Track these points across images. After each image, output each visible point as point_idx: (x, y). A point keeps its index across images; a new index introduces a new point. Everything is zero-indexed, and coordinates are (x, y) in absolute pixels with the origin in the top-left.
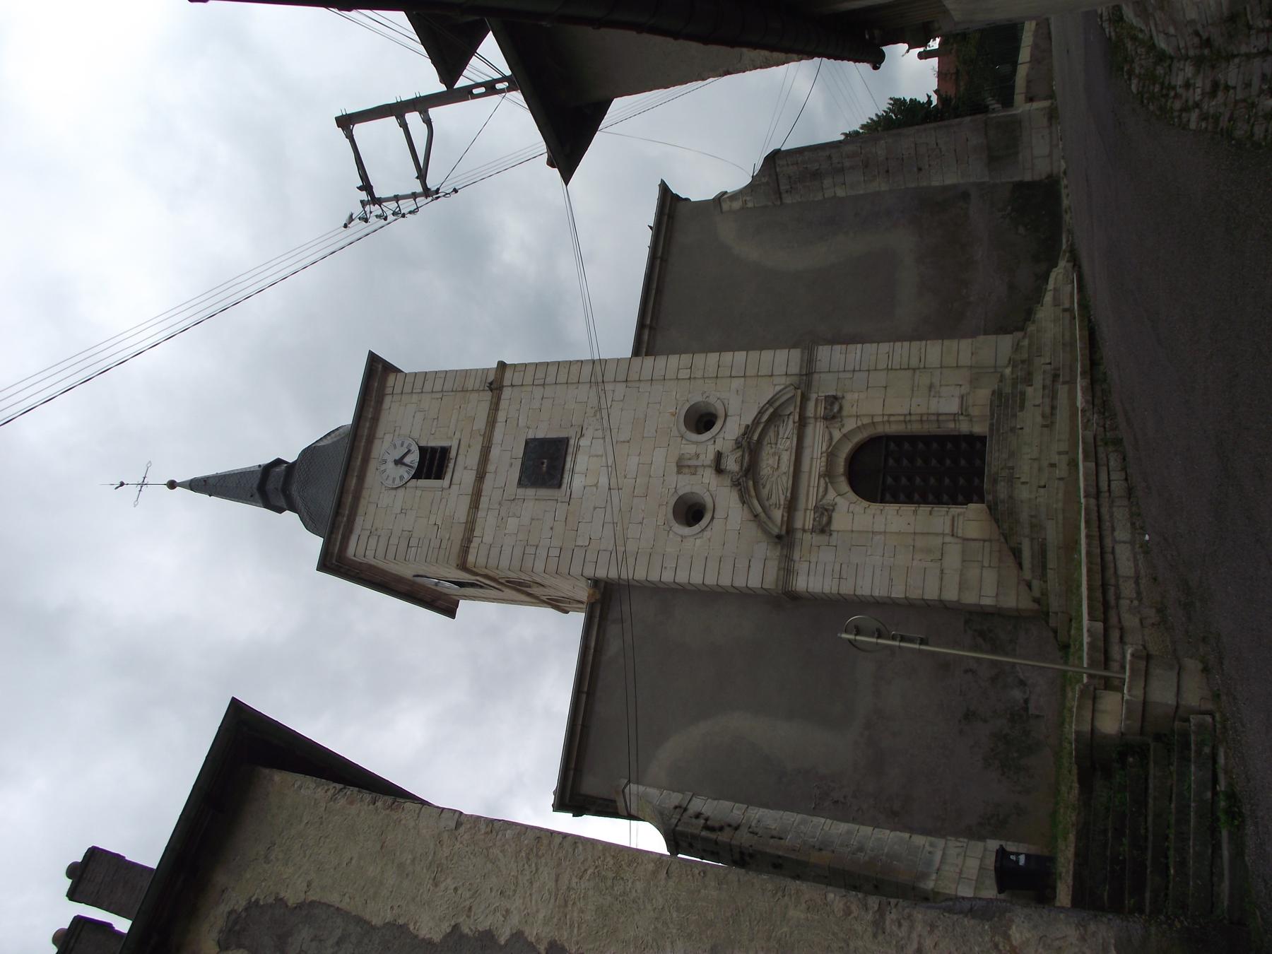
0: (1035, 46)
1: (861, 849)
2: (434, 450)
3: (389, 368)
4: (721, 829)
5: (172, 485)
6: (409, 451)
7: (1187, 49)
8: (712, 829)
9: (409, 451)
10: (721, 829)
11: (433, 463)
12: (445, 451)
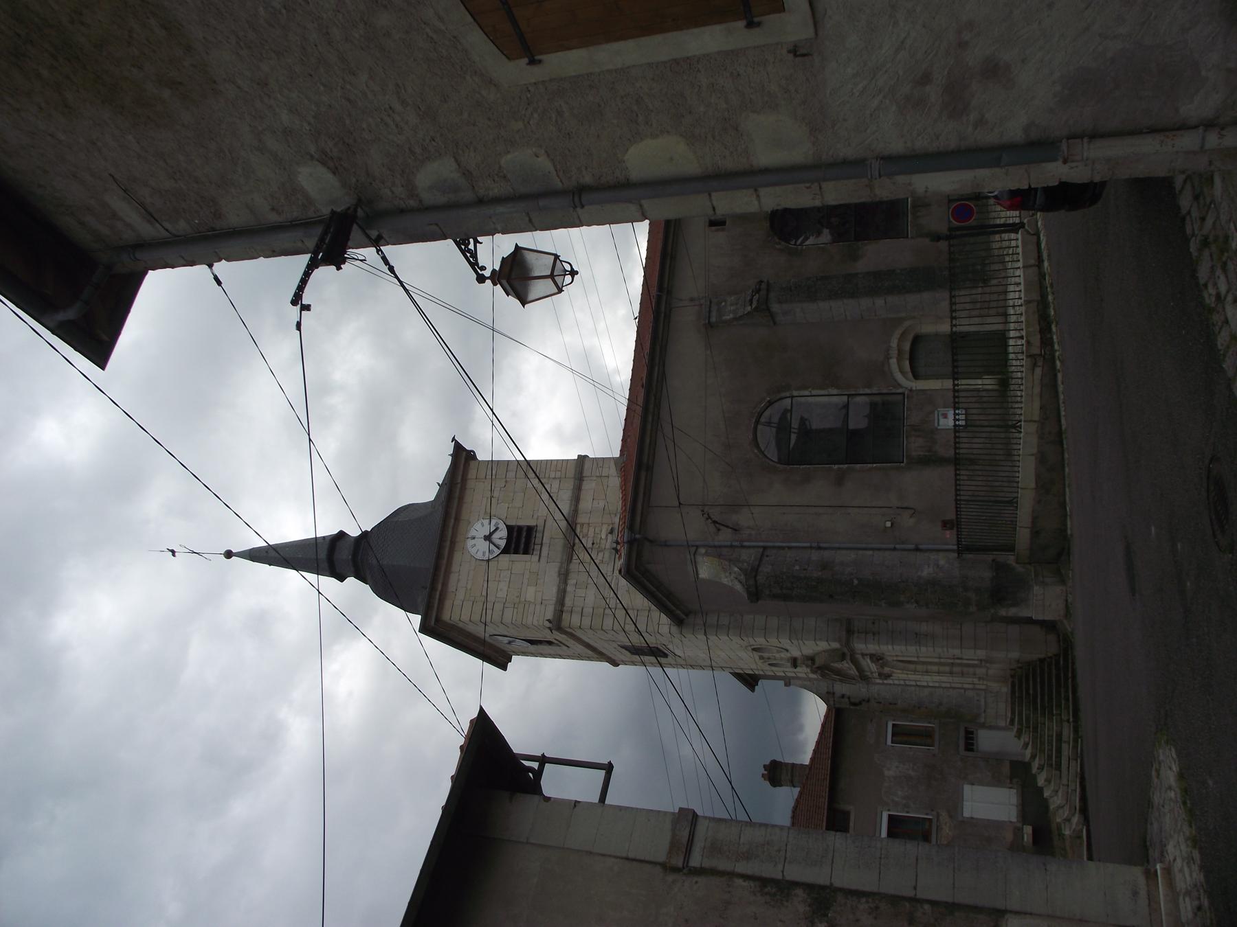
0: (1042, 458)
1: (941, 704)
2: (520, 528)
3: (471, 456)
4: (860, 703)
5: (229, 554)
6: (497, 529)
7: (1014, 306)
8: (854, 704)
9: (497, 529)
10: (860, 703)
11: (520, 540)
12: (530, 530)
